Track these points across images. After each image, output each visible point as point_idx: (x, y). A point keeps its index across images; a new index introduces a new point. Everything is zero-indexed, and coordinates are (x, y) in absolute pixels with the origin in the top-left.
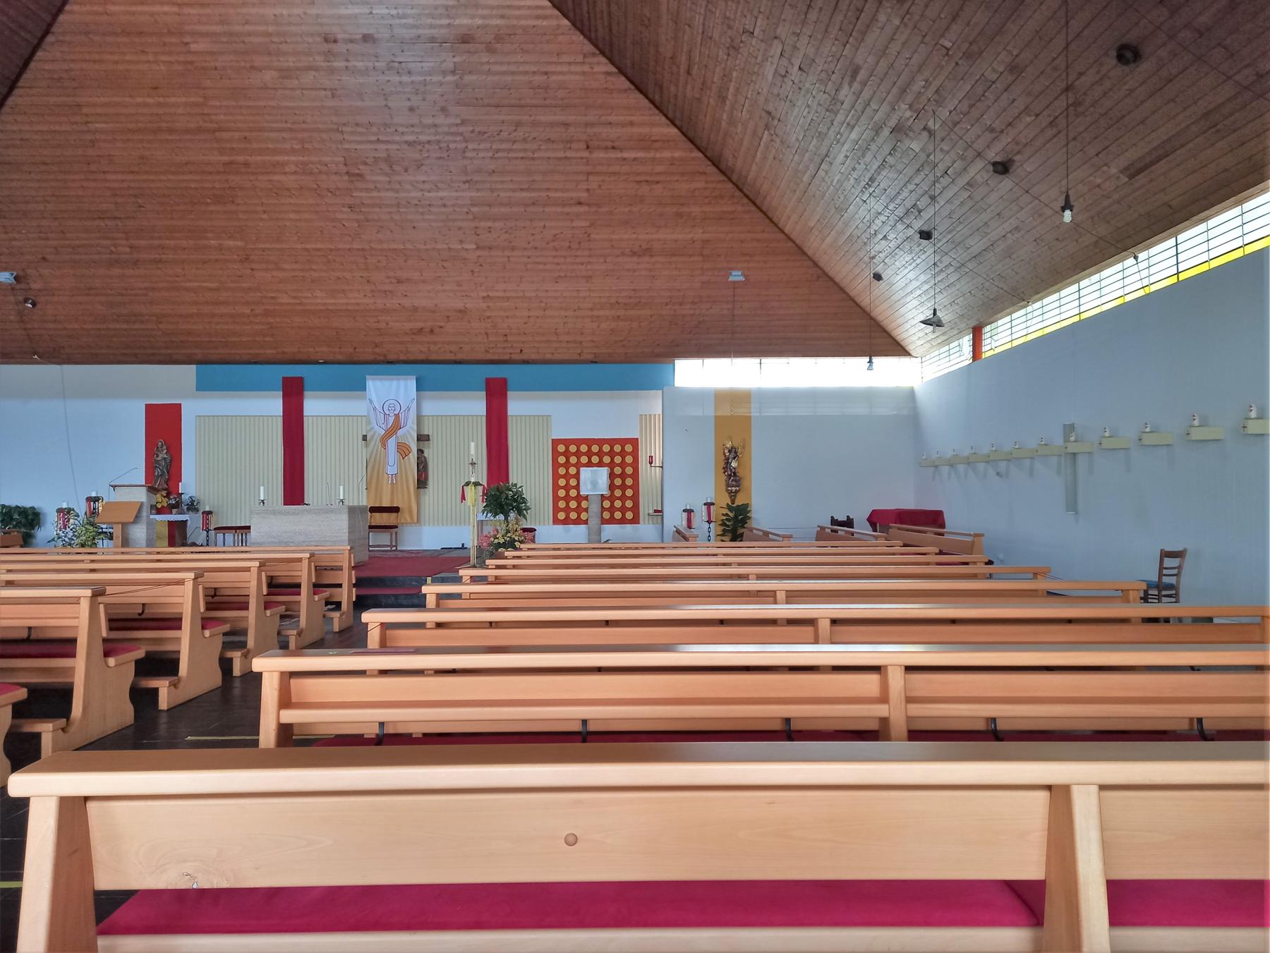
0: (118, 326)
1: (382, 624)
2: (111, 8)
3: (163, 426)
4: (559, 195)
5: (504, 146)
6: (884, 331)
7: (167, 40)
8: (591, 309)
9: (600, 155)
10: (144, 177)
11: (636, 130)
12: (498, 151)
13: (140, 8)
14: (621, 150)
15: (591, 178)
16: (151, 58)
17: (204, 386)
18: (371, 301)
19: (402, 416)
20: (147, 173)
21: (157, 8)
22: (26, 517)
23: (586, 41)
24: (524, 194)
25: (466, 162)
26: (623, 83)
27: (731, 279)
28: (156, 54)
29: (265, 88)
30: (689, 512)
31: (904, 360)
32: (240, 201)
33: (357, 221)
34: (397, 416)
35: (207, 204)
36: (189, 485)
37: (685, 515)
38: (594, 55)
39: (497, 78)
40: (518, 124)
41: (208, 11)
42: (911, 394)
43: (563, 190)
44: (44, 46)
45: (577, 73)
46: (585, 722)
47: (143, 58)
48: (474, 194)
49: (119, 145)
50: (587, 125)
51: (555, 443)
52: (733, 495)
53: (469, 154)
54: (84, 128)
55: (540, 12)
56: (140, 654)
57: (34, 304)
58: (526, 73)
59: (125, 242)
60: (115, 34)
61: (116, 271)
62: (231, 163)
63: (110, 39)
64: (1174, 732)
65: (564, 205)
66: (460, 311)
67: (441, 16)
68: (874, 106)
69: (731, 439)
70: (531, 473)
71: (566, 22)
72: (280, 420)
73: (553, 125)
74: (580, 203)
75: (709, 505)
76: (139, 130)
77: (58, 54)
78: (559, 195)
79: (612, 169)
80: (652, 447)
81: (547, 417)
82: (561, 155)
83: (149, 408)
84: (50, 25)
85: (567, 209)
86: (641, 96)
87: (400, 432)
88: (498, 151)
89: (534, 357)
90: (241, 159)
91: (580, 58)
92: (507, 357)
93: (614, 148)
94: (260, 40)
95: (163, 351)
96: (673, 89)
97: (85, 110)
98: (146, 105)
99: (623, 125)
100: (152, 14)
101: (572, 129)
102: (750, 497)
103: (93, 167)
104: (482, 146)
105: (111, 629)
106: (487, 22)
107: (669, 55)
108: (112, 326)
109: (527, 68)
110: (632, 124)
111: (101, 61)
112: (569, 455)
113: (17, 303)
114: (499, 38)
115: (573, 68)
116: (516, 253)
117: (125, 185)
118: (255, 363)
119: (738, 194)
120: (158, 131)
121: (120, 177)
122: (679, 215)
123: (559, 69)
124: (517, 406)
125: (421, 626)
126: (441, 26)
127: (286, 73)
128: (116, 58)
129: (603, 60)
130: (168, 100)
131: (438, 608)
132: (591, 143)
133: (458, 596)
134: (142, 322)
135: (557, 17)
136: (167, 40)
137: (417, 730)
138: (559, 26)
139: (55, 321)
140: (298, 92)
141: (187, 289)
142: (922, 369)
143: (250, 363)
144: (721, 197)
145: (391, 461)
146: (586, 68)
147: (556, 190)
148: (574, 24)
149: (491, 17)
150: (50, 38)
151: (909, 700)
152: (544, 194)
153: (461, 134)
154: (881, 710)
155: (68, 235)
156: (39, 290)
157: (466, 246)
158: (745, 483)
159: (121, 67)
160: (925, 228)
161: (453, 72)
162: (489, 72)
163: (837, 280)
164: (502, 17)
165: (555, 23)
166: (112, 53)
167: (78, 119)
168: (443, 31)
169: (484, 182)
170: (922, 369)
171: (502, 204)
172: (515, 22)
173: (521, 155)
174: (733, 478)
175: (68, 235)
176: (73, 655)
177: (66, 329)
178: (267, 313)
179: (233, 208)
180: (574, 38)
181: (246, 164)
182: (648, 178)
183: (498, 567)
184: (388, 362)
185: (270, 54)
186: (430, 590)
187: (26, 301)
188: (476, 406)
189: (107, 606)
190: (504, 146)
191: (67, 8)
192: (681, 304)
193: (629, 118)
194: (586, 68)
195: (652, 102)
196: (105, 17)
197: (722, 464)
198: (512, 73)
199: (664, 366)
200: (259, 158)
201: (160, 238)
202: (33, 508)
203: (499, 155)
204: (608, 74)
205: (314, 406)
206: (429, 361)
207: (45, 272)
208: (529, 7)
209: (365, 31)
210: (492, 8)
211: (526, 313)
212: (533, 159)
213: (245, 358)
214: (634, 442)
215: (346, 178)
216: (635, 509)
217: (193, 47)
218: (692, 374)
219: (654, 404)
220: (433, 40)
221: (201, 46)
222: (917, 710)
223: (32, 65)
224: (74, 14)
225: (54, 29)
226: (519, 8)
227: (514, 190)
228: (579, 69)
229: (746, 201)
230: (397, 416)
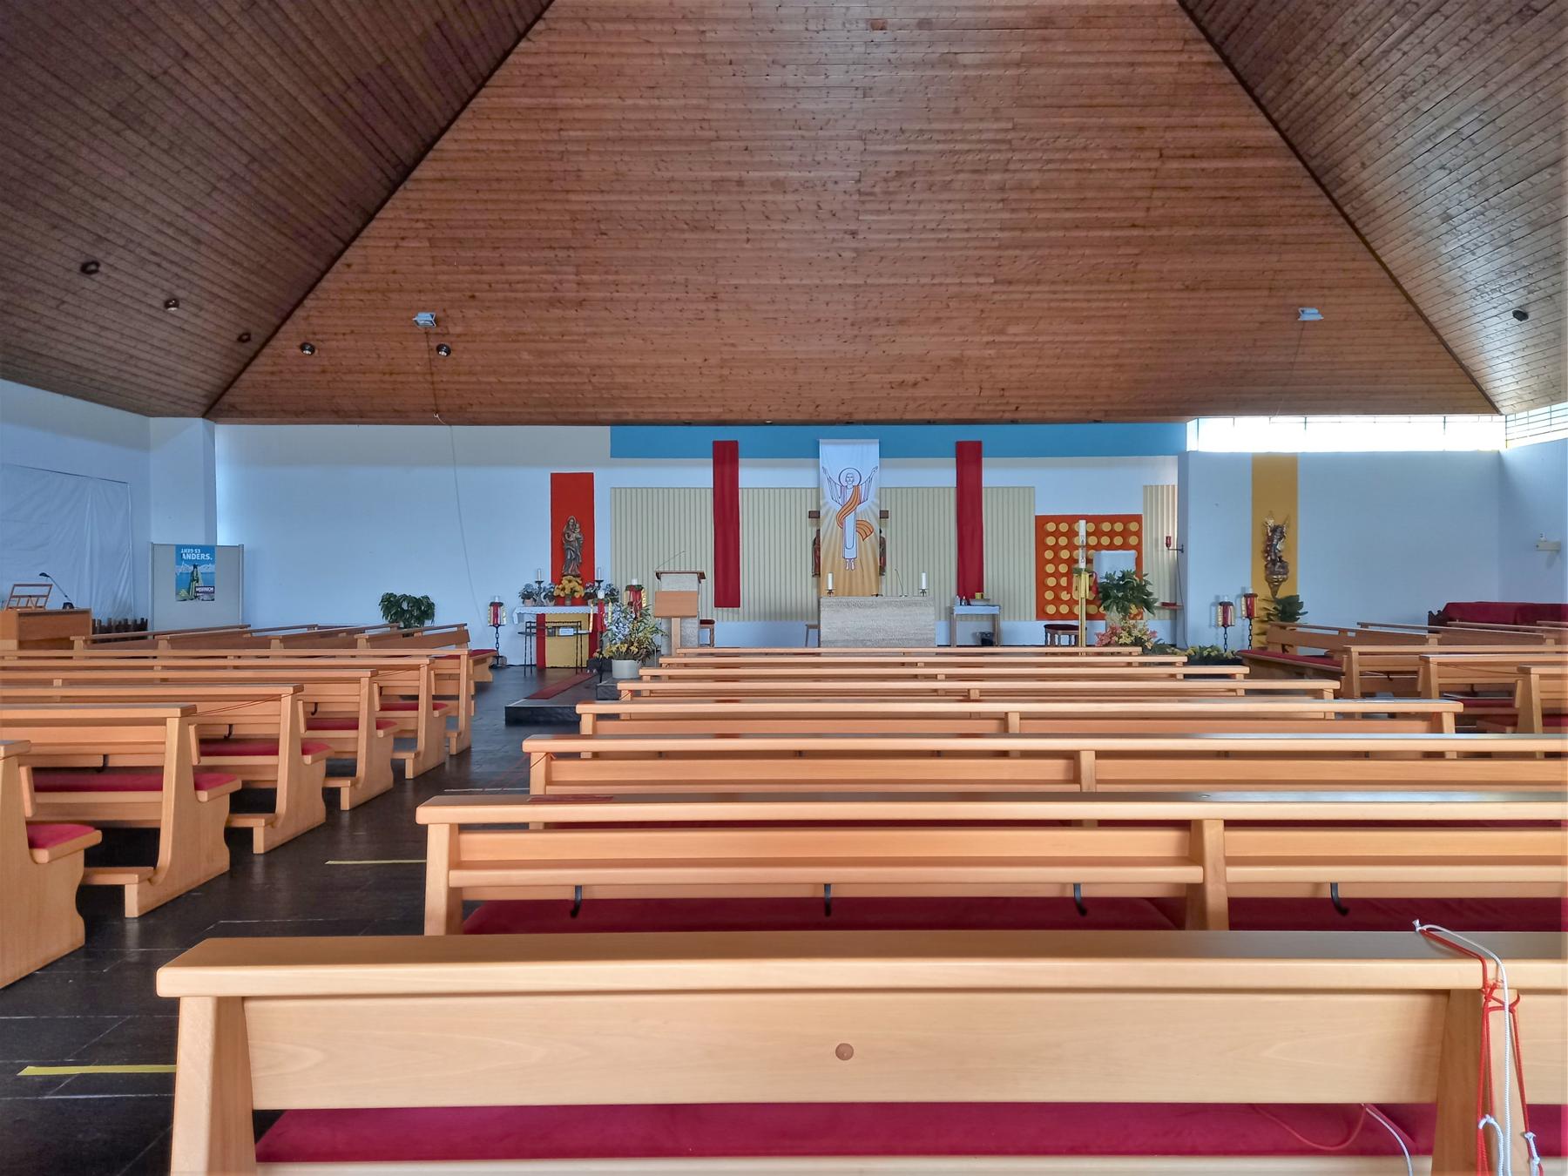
0: (543, 379)
3: (572, 499)
6: (1474, 382)
15: (1156, 194)
19: (863, 488)
20: (622, 192)
30: (1225, 606)
34: (856, 488)
37: (1220, 609)
38: (1198, 41)
39: (1070, 71)
48: (1006, 215)
49: (593, 157)
50: (1168, 128)
51: (1041, 521)
52: (1274, 586)
53: (1012, 167)
56: (237, 785)
57: (448, 352)
59: (572, 277)
61: (557, 312)
62: (723, 180)
63: (610, 27)
69: (1271, 515)
70: (1010, 562)
73: (1123, 129)
74: (1134, 226)
78: (1112, 215)
80: (1162, 526)
81: (1032, 487)
83: (555, 478)
87: (860, 508)
90: (734, 174)
93: (1193, 157)
96: (1311, 82)
97: (561, 115)
98: (636, 108)
101: (1147, 133)
103: (555, 185)
105: (203, 753)
108: (536, 379)
110: (1222, 126)
119: (1335, 211)
122: (1255, 239)
124: (994, 475)
128: (613, 49)
129: (1207, 47)
131: (594, 736)
136: (679, 27)
139: (470, 373)
144: (1311, 216)
146: (1184, 57)
150: (539, 26)
156: (459, 336)
159: (616, 61)
167: (550, 126)
171: (1038, 229)
173: (1075, 166)
174: (1275, 564)
176: (160, 788)
180: (1178, 20)
182: (1226, 194)
183: (655, 678)
184: (847, 423)
186: (587, 710)
187: (439, 349)
188: (944, 475)
189: (199, 727)
193: (1221, 120)
194: (1184, 57)
197: (1261, 547)
199: (1173, 427)
200: (757, 174)
204: (1209, 64)
205: (750, 476)
214: (1041, 521)
217: (710, 36)
218: (1215, 436)
219: (1167, 474)
221: (724, 32)
223: (511, 58)
225: (546, 15)
228: (1175, 58)
229: (1341, 220)
230: (856, 488)
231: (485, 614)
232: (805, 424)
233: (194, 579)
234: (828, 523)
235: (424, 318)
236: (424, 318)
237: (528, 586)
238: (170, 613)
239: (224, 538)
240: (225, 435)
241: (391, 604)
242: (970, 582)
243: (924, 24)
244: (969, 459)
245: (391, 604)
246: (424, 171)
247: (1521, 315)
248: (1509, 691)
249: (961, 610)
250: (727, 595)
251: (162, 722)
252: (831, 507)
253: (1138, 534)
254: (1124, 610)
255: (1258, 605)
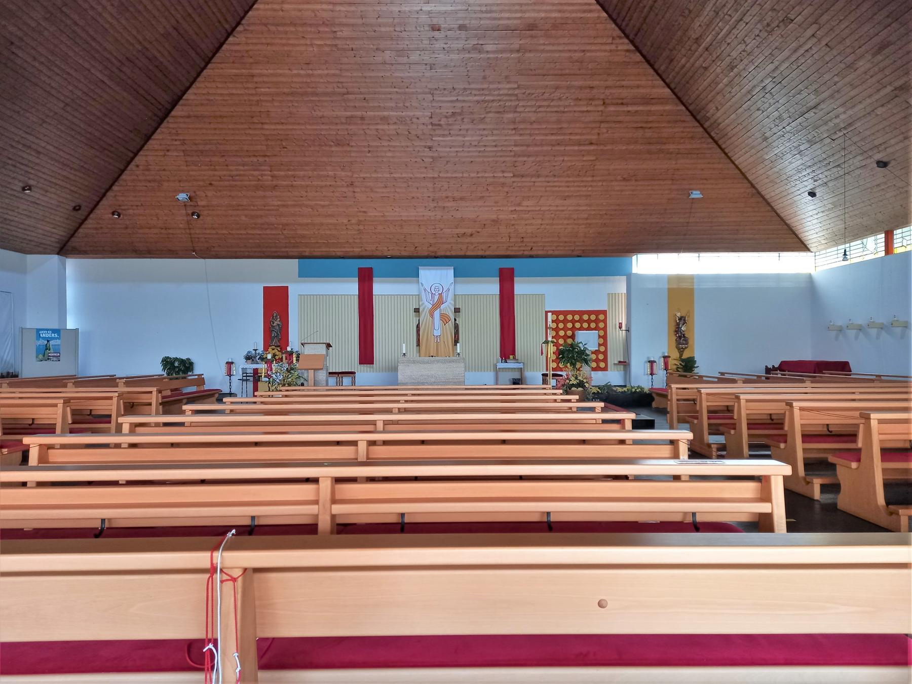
1: (40, 445)
2: (286, 6)
3: (276, 301)
4: (578, 137)
5: (545, 103)
6: (794, 233)
7: (321, 29)
8: (587, 219)
9: (612, 108)
10: (291, 127)
11: (641, 91)
12: (540, 107)
13: (305, 6)
14: (627, 104)
15: (602, 125)
16: (308, 42)
17: (303, 274)
18: (433, 214)
19: (444, 295)
20: (294, 124)
21: (318, 7)
22: (185, 366)
23: (616, 28)
24: (553, 137)
25: (516, 115)
26: (638, 57)
27: (693, 196)
28: (312, 39)
29: (385, 63)
30: (652, 363)
31: (809, 254)
32: (353, 144)
33: (432, 157)
34: (440, 295)
35: (331, 146)
36: (294, 344)
37: (649, 365)
38: (620, 38)
40: (557, 88)
41: (353, 8)
42: (810, 279)
43: (581, 134)
44: (235, 33)
45: (605, 51)
46: (253, 518)
47: (302, 42)
54: (254, 92)
55: (586, 7)
57: (198, 216)
58: (570, 51)
60: (285, 25)
62: (352, 117)
63: (281, 29)
64: (600, 523)
65: (580, 145)
66: (493, 221)
67: (516, 11)
68: (887, 72)
69: (679, 310)
70: (532, 337)
71: (605, 15)
72: (498, 297)
73: (581, 88)
74: (591, 144)
75: (666, 358)
76: (292, 94)
77: (244, 39)
78: (578, 137)
79: (620, 118)
80: (618, 316)
81: (545, 295)
82: (585, 109)
83: (266, 289)
84: (242, 18)
85: (582, 148)
86: (648, 66)
87: (442, 306)
88: (540, 107)
89: (540, 253)
90: (359, 113)
91: (610, 41)
92: (521, 253)
93: (622, 104)
94: (388, 29)
95: (283, 250)
96: (683, 61)
98: (299, 75)
99: (631, 87)
100: (313, 11)
102: (693, 352)
104: (529, 104)
106: (549, 15)
107: (694, 36)
109: (570, 47)
110: (638, 87)
111: (272, 44)
112: (567, 322)
113: (187, 215)
114: (555, 26)
115: (604, 47)
116: (540, 179)
117: (275, 132)
118: (436, 257)
120: (306, 94)
121: (273, 127)
123: (593, 48)
124: (521, 288)
125: (118, 446)
126: (516, 18)
127: (401, 52)
129: (626, 41)
130: (315, 72)
131: (384, 432)
132: (607, 101)
133: (181, 424)
134: (272, 229)
135: (599, 11)
136: (321, 29)
137: (28, 526)
138: (599, 17)
140: (407, 66)
141: (307, 206)
142: (821, 261)
143: (343, 258)
145: (436, 327)
146: (613, 47)
147: (576, 134)
148: (610, 16)
149: (551, 11)
150: (240, 28)
151: (334, 501)
152: (567, 137)
153: (516, 95)
154: (314, 509)
155: (230, 168)
156: (204, 206)
157: (506, 175)
158: (690, 342)
159: (286, 48)
160: (885, 160)
161: (518, 51)
162: (543, 51)
163: (767, 197)
164: (560, 11)
165: (596, 15)
166: (281, 39)
167: (250, 85)
168: (515, 22)
169: (526, 129)
170: (821, 261)
171: (536, 145)
172: (568, 15)
173: (555, 109)
174: (681, 339)
175: (230, 168)
177: (217, 233)
178: (359, 223)
179: (349, 149)
180: (608, 26)
181: (362, 118)
184: (434, 257)
185: (392, 39)
187: (193, 214)
188: (492, 288)
190: (545, 103)
191: (255, 6)
192: (651, 215)
194: (613, 47)
195: (656, 71)
196: (281, 13)
197: (673, 329)
198: (560, 51)
200: (372, 113)
201: (294, 170)
202: (188, 359)
203: (540, 109)
204: (627, 51)
205: (380, 288)
206: (461, 257)
207: (210, 194)
208: (580, 4)
209: (461, 22)
210: (554, 4)
211: (540, 222)
212: (564, 112)
213: (318, 254)
214: (604, 312)
215: (430, 127)
216: (605, 360)
217: (339, 34)
218: (649, 265)
219: (620, 286)
220: (507, 28)
221: (346, 32)
222: (337, 509)
224: (260, 10)
225: (243, 22)
226: (572, 4)
227: (546, 135)
228: (608, 48)
229: (710, 140)
230: (440, 295)
231: (224, 369)
232: (411, 258)
233: (47, 348)
234: (425, 314)
235: (182, 196)
236: (182, 196)
237: (249, 352)
238: (32, 368)
239: (71, 324)
240: (72, 265)
241: (168, 363)
242: (508, 349)
243: (462, 28)
244: (507, 279)
245: (168, 363)
246: (177, 111)
247: (812, 194)
248: (729, 409)
249: (501, 365)
250: (366, 356)
251: (55, 405)
252: (426, 305)
253: (605, 321)
254: (573, 365)
255: (671, 362)
